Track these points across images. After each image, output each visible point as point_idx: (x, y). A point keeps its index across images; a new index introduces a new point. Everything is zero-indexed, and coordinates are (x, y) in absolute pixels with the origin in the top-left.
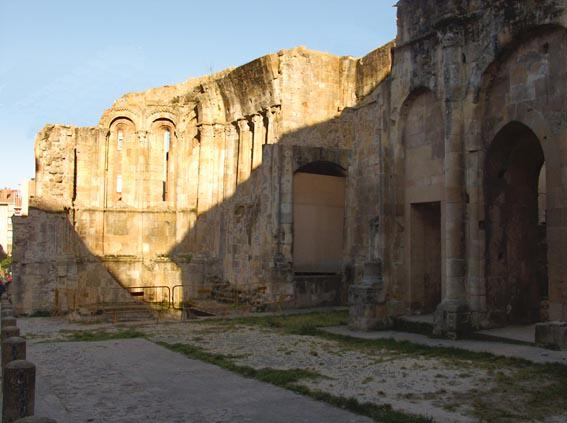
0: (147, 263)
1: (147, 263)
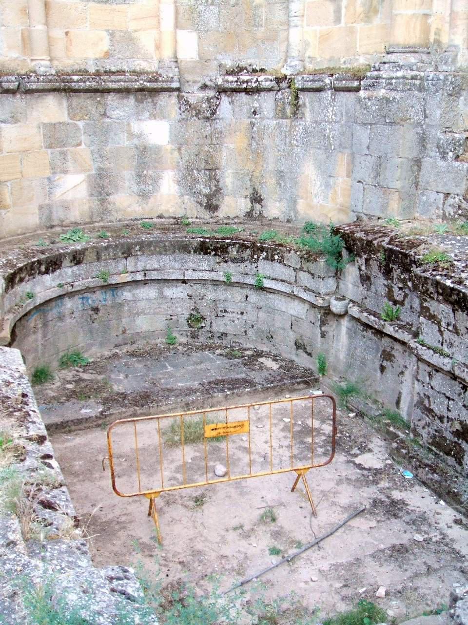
0: (195, 96)
1: (195, 96)
